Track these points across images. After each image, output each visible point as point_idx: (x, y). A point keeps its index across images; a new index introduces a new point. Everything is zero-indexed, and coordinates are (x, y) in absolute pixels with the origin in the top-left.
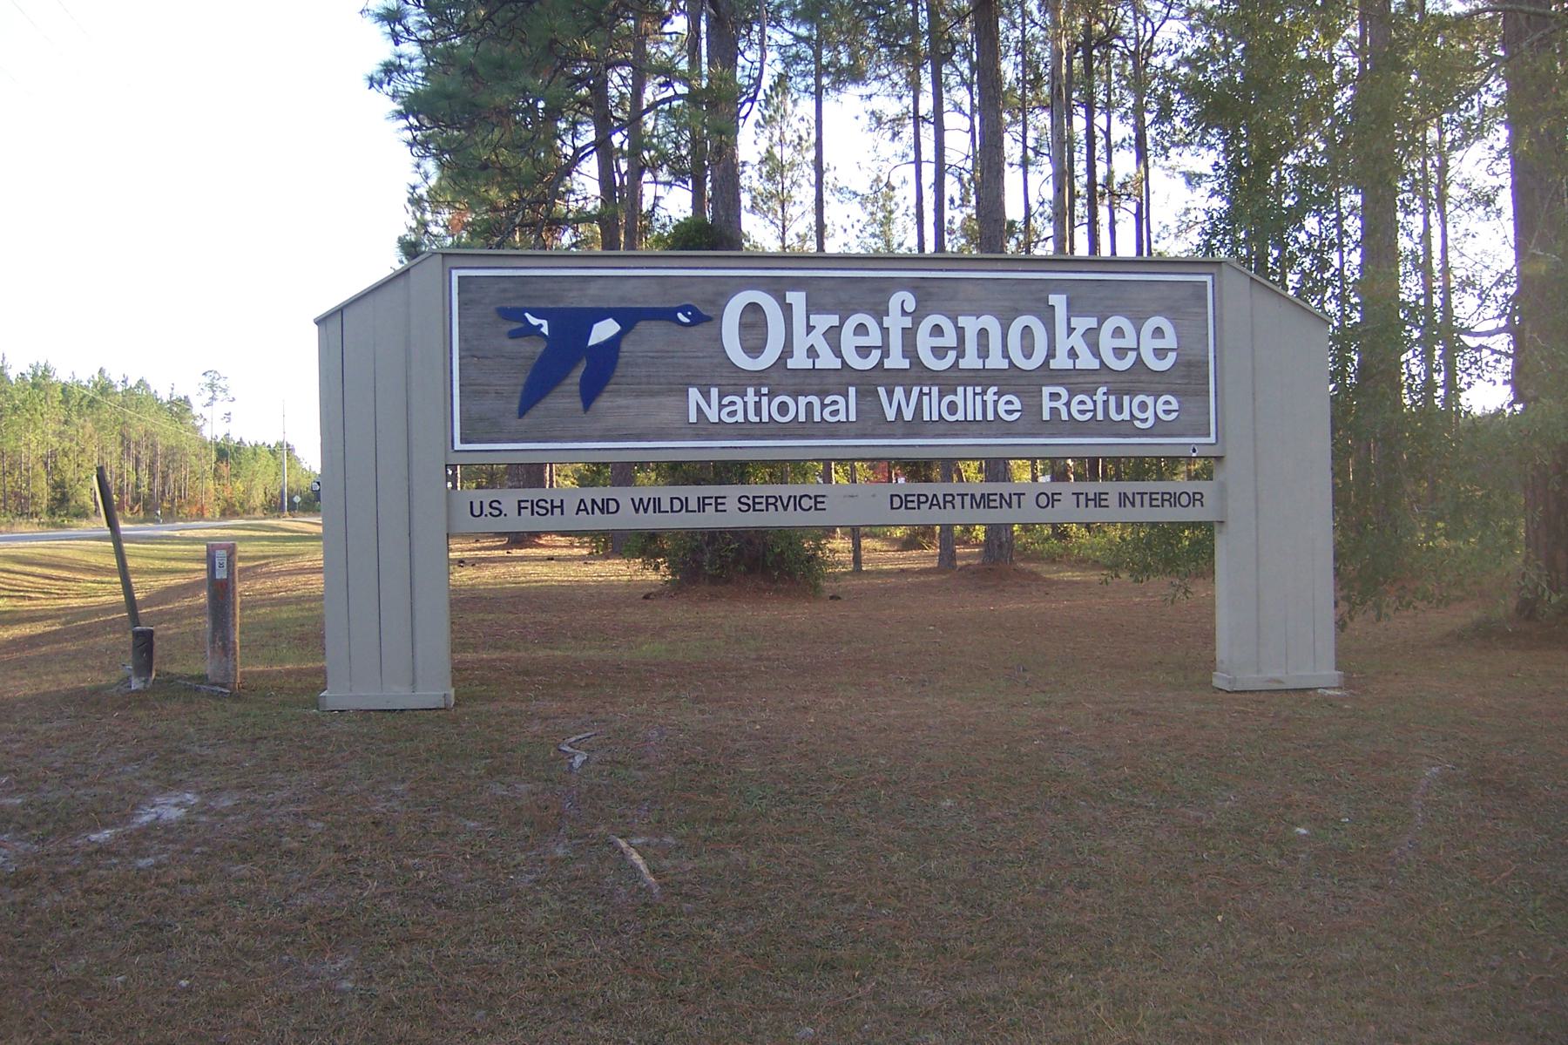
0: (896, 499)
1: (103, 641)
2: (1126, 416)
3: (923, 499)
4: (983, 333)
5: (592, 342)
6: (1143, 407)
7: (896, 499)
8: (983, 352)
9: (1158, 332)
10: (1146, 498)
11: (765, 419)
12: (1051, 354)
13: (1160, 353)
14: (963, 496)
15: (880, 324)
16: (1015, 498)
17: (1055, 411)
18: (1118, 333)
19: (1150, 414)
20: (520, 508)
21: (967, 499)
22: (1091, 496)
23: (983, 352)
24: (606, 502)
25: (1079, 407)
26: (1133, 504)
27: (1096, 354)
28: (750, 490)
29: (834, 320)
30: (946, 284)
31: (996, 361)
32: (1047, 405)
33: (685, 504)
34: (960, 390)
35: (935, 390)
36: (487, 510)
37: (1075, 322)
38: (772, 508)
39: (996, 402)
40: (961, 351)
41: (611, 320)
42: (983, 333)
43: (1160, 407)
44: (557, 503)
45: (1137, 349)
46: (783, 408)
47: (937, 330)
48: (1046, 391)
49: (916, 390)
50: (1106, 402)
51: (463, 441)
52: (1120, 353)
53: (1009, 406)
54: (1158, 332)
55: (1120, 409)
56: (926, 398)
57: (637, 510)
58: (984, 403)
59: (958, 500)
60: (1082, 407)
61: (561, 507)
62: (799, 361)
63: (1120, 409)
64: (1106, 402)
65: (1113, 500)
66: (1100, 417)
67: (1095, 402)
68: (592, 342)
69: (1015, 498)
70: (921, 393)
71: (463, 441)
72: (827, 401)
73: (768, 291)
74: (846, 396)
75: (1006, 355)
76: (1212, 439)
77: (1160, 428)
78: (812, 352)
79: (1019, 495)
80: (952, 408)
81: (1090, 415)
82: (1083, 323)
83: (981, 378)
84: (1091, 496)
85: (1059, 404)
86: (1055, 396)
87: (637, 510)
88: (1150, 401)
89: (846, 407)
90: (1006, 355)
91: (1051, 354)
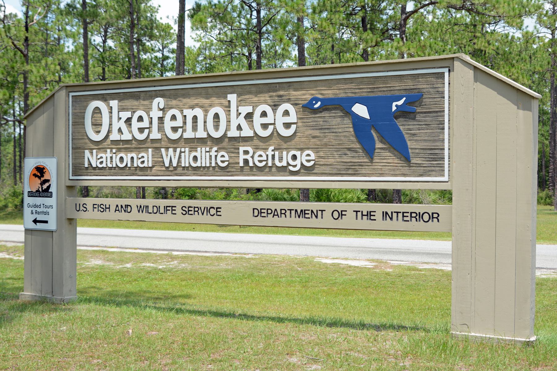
0: (256, 211)
1: (20, 264)
2: (284, 163)
3: (269, 211)
4: (195, 118)
5: (369, 118)
6: (294, 157)
7: (256, 211)
8: (195, 128)
9: (286, 113)
10: (400, 215)
11: (114, 166)
12: (228, 129)
13: (287, 126)
14: (291, 210)
15: (149, 115)
16: (320, 213)
17: (246, 162)
18: (264, 114)
19: (298, 162)
20: (94, 208)
21: (293, 212)
22: (365, 213)
23: (195, 128)
24: (127, 206)
25: (258, 158)
26: (391, 219)
27: (252, 127)
28: (260, 205)
29: (249, 109)
30: (245, 87)
31: (201, 134)
32: (242, 157)
33: (158, 208)
34: (199, 149)
35: (187, 149)
36: (82, 208)
37: (241, 109)
38: (414, 219)
39: (216, 156)
40: (184, 128)
41: (357, 104)
42: (195, 118)
43: (304, 158)
44: (108, 206)
45: (274, 124)
46: (122, 159)
47: (174, 118)
48: (242, 149)
49: (178, 150)
50: (273, 156)
51: (443, 175)
52: (265, 126)
53: (222, 158)
54: (286, 113)
55: (281, 159)
56: (183, 154)
57: (139, 211)
58: (211, 156)
59: (288, 213)
60: (308, 158)
61: (109, 208)
62: (115, 136)
63: (281, 159)
64: (273, 156)
65: (378, 216)
66: (270, 164)
67: (267, 155)
68: (369, 118)
69: (320, 213)
70: (181, 152)
71: (443, 175)
72: (140, 156)
73: (99, 100)
74: (148, 153)
75: (205, 129)
76: (71, 178)
77: (306, 170)
78: (239, 128)
79: (322, 211)
80: (195, 158)
81: (264, 163)
82: (125, 115)
83: (208, 141)
84: (365, 213)
85: (248, 157)
86: (246, 152)
87: (139, 211)
88: (298, 153)
89: (147, 158)
90: (205, 129)
91: (228, 129)
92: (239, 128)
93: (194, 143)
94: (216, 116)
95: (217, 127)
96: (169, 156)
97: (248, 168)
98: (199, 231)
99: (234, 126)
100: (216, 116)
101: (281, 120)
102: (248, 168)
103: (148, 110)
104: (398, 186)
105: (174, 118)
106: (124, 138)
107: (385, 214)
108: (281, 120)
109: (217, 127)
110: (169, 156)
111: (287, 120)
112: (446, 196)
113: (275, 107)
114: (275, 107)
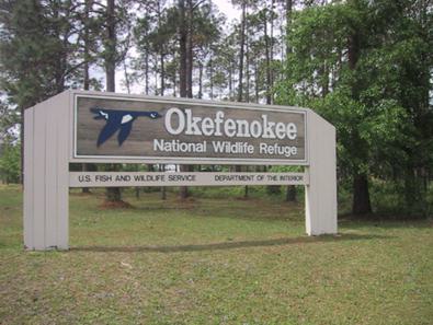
4: (243, 126)
8: (244, 132)
9: (292, 128)
12: (262, 133)
13: (292, 134)
18: (281, 127)
23: (244, 132)
25: (270, 150)
27: (201, 129)
42: (243, 126)
52: (281, 134)
53: (251, 149)
77: (292, 157)
78: (193, 129)
83: (243, 140)
89: (203, 147)
91: (262, 133)
92: (268, 133)
93: (233, 140)
94: (256, 126)
95: (256, 132)
96: (219, 147)
97: (264, 155)
98: (70, 202)
99: (189, 128)
100: (256, 126)
101: (289, 131)
102: (264, 155)
103: (214, 118)
104: (138, 162)
105: (230, 124)
106: (196, 133)
107: (143, 179)
108: (289, 131)
109: (256, 132)
110: (219, 147)
111: (208, 126)
112: (74, 167)
113: (286, 124)
114: (286, 124)
